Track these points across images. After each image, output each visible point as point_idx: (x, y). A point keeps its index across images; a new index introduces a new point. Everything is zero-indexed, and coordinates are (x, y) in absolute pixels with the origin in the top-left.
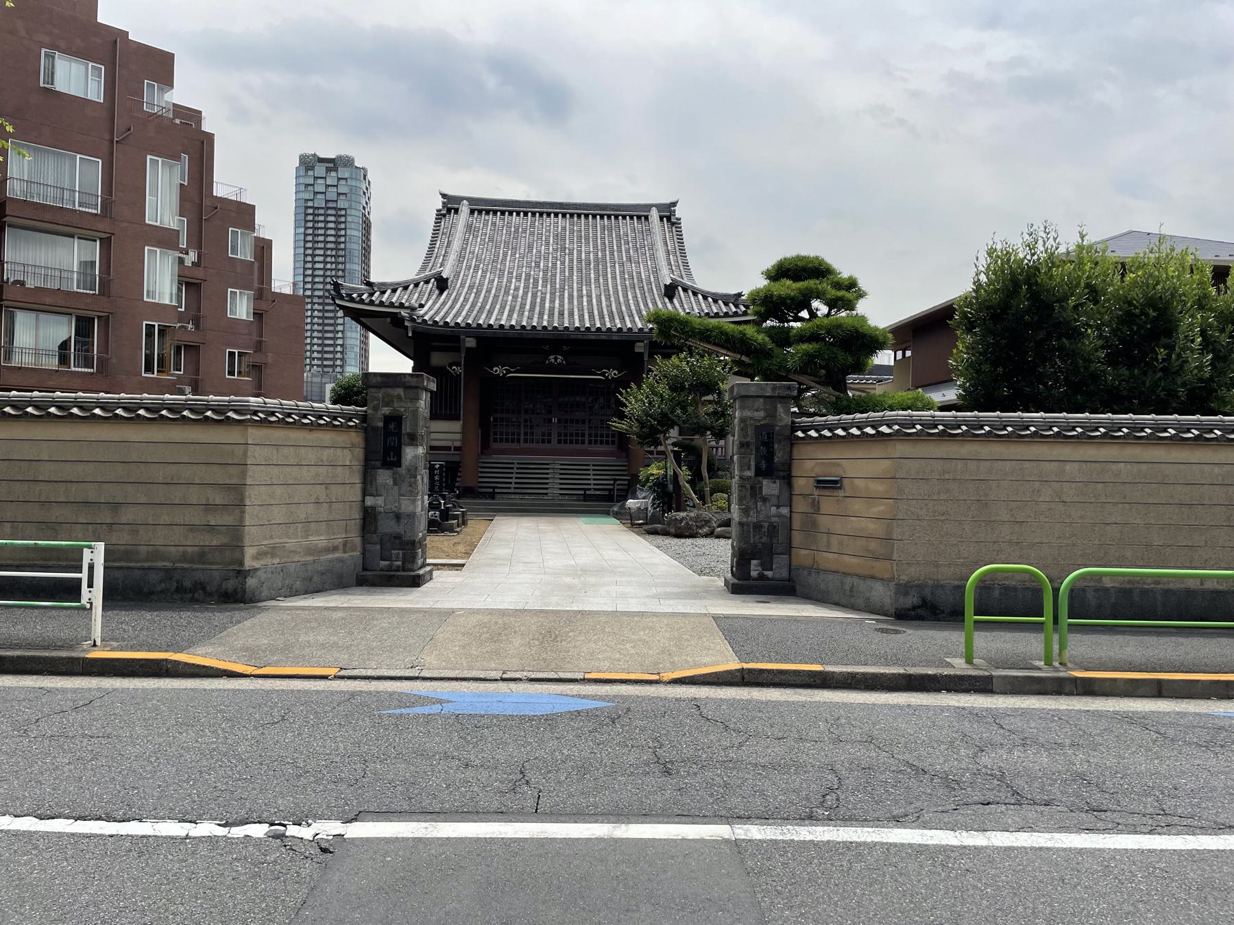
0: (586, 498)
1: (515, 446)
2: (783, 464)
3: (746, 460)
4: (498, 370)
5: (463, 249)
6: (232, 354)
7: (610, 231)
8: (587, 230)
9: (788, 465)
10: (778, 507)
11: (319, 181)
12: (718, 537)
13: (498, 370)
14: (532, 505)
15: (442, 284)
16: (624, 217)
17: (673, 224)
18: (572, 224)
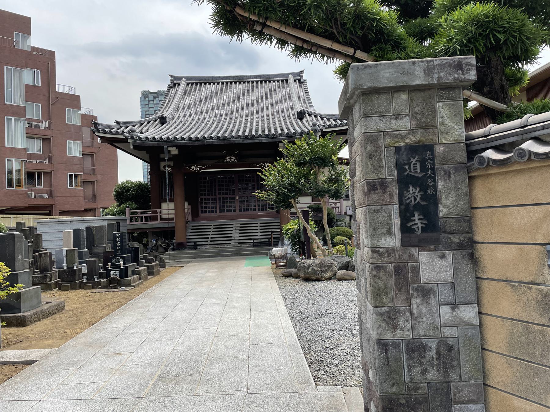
0: (255, 245)
1: (214, 215)
2: (459, 219)
3: (382, 217)
4: (194, 168)
5: (180, 103)
6: (71, 176)
7: (266, 88)
8: (253, 89)
9: (466, 222)
10: (454, 305)
11: (151, 102)
12: (340, 280)
13: (194, 168)
14: (220, 252)
15: (163, 120)
16: (274, 81)
17: (302, 83)
18: (244, 87)
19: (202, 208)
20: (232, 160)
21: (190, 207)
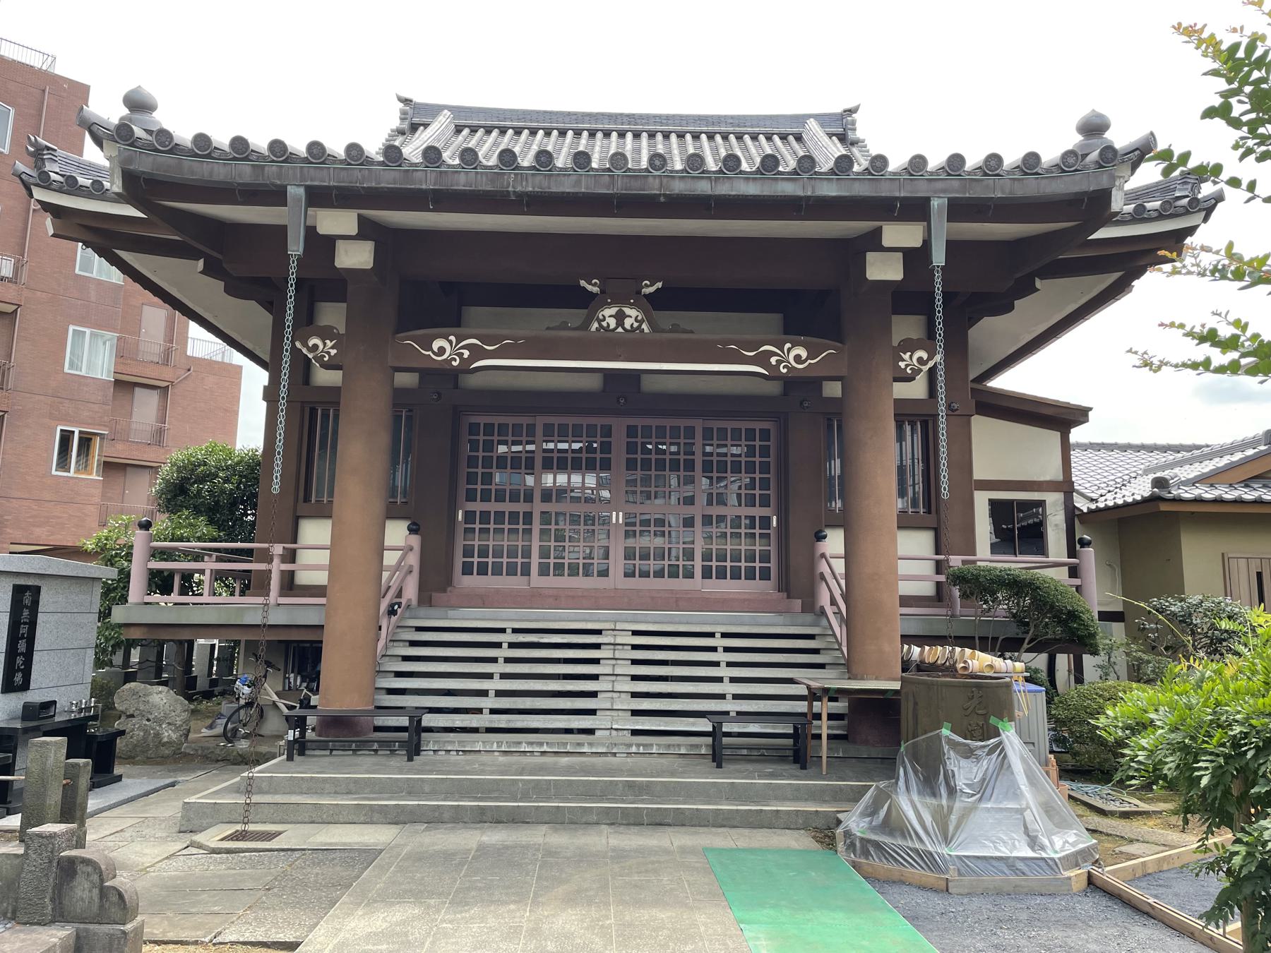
6: (66, 438)
19: (468, 552)
20: (628, 323)
21: (415, 540)
